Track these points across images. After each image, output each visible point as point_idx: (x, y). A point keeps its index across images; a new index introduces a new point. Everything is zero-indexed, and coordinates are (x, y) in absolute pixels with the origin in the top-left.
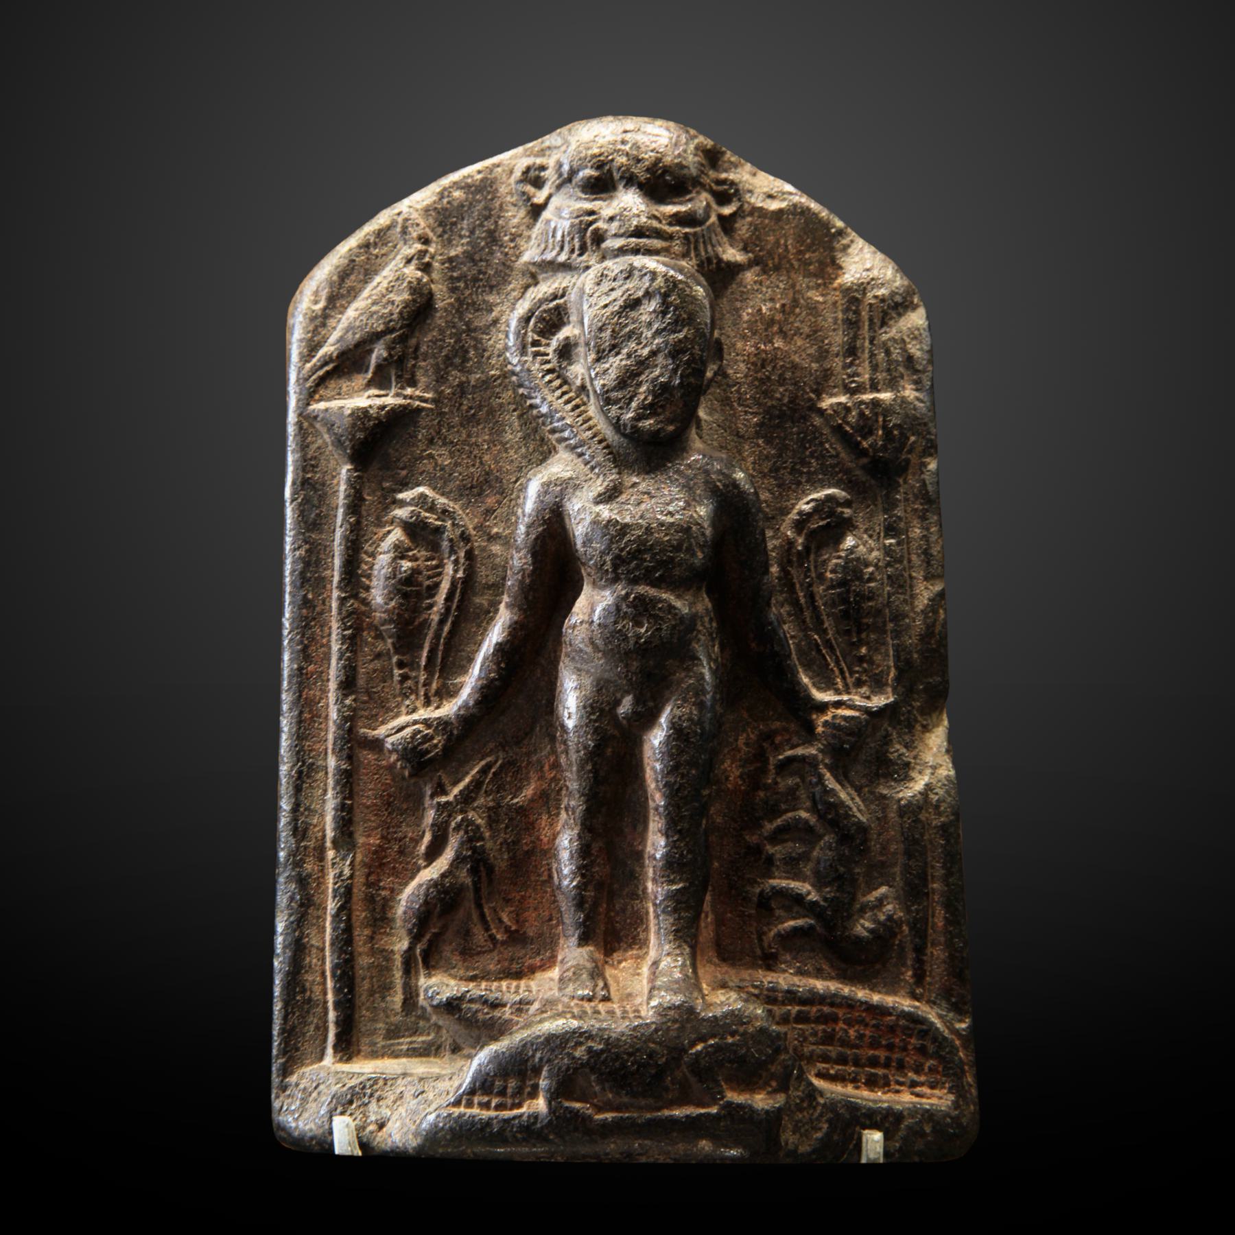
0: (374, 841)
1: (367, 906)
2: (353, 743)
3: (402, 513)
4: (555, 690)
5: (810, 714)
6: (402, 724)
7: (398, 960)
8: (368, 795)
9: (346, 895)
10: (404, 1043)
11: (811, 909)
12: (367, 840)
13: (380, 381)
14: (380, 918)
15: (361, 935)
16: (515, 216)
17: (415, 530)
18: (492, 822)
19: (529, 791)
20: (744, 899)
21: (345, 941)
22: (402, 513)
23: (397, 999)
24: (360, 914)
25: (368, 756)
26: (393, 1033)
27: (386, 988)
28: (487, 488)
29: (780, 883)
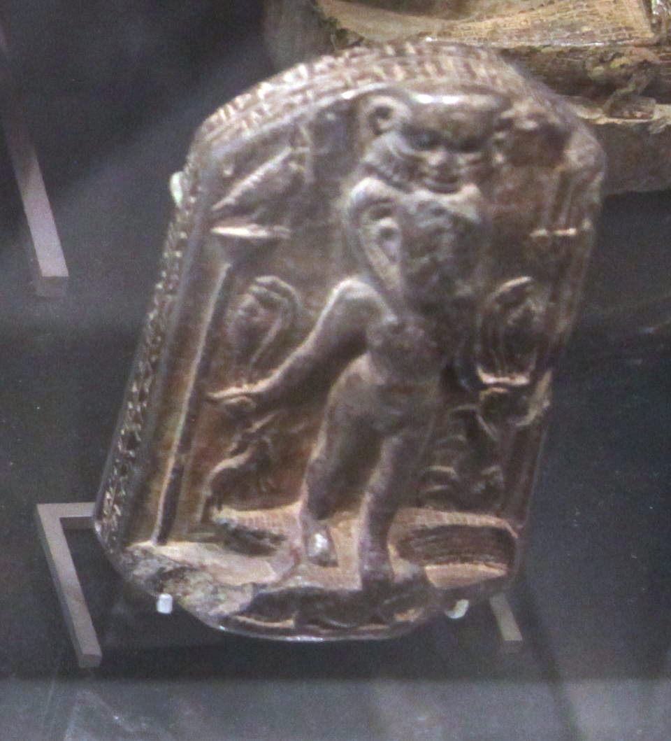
0: (203, 445)
1: (190, 475)
2: (200, 399)
3: (255, 289)
4: (58, 231)
5: (317, 531)
6: (233, 392)
7: (203, 500)
8: (204, 423)
9: (178, 471)
10: (197, 535)
11: (453, 483)
12: (197, 444)
13: (261, 222)
14: (197, 478)
15: (184, 485)
16: (365, 132)
17: (265, 301)
18: (275, 443)
19: (301, 427)
20: (610, 15)
21: (175, 486)
22: (255, 289)
23: (198, 516)
24: (186, 479)
25: (208, 407)
26: (193, 530)
27: (192, 510)
28: (315, 284)
29: (437, 468)
